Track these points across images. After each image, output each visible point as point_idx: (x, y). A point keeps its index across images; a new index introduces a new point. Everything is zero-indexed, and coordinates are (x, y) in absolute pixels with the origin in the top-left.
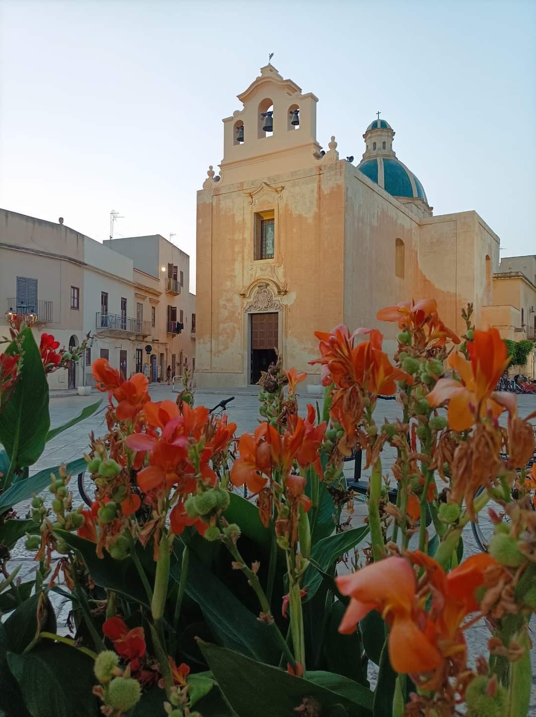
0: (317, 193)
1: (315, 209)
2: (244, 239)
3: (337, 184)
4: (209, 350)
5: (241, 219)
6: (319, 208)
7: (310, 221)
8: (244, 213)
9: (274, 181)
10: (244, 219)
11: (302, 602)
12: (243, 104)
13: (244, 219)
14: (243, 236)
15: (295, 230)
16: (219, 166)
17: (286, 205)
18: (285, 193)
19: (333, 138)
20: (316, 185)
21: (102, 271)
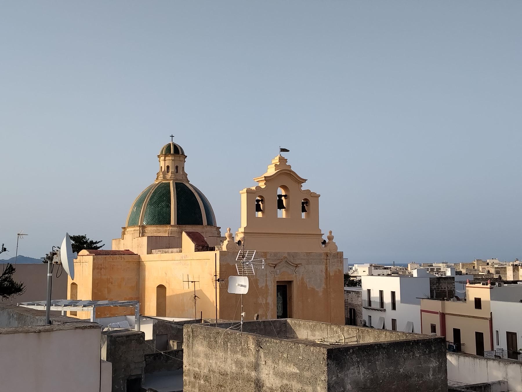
0: (325, 273)
1: (324, 285)
2: (267, 304)
3: (339, 270)
4: (352, 341)
5: (264, 285)
6: (326, 285)
7: (321, 294)
8: (266, 280)
9: (293, 257)
10: (266, 285)
11: (485, 285)
12: (317, 194)
13: (266, 285)
14: (266, 300)
15: (309, 300)
16: (220, 228)
17: (302, 279)
18: (301, 269)
19: (331, 232)
20: (324, 267)
21: (97, 328)
